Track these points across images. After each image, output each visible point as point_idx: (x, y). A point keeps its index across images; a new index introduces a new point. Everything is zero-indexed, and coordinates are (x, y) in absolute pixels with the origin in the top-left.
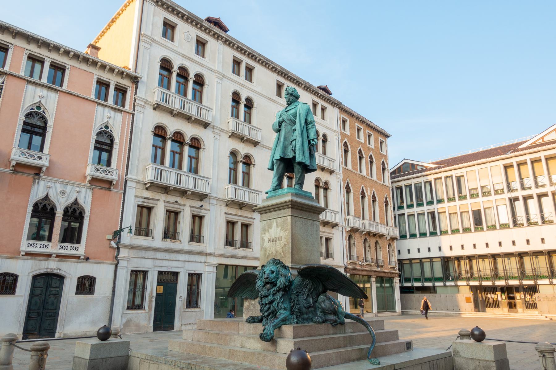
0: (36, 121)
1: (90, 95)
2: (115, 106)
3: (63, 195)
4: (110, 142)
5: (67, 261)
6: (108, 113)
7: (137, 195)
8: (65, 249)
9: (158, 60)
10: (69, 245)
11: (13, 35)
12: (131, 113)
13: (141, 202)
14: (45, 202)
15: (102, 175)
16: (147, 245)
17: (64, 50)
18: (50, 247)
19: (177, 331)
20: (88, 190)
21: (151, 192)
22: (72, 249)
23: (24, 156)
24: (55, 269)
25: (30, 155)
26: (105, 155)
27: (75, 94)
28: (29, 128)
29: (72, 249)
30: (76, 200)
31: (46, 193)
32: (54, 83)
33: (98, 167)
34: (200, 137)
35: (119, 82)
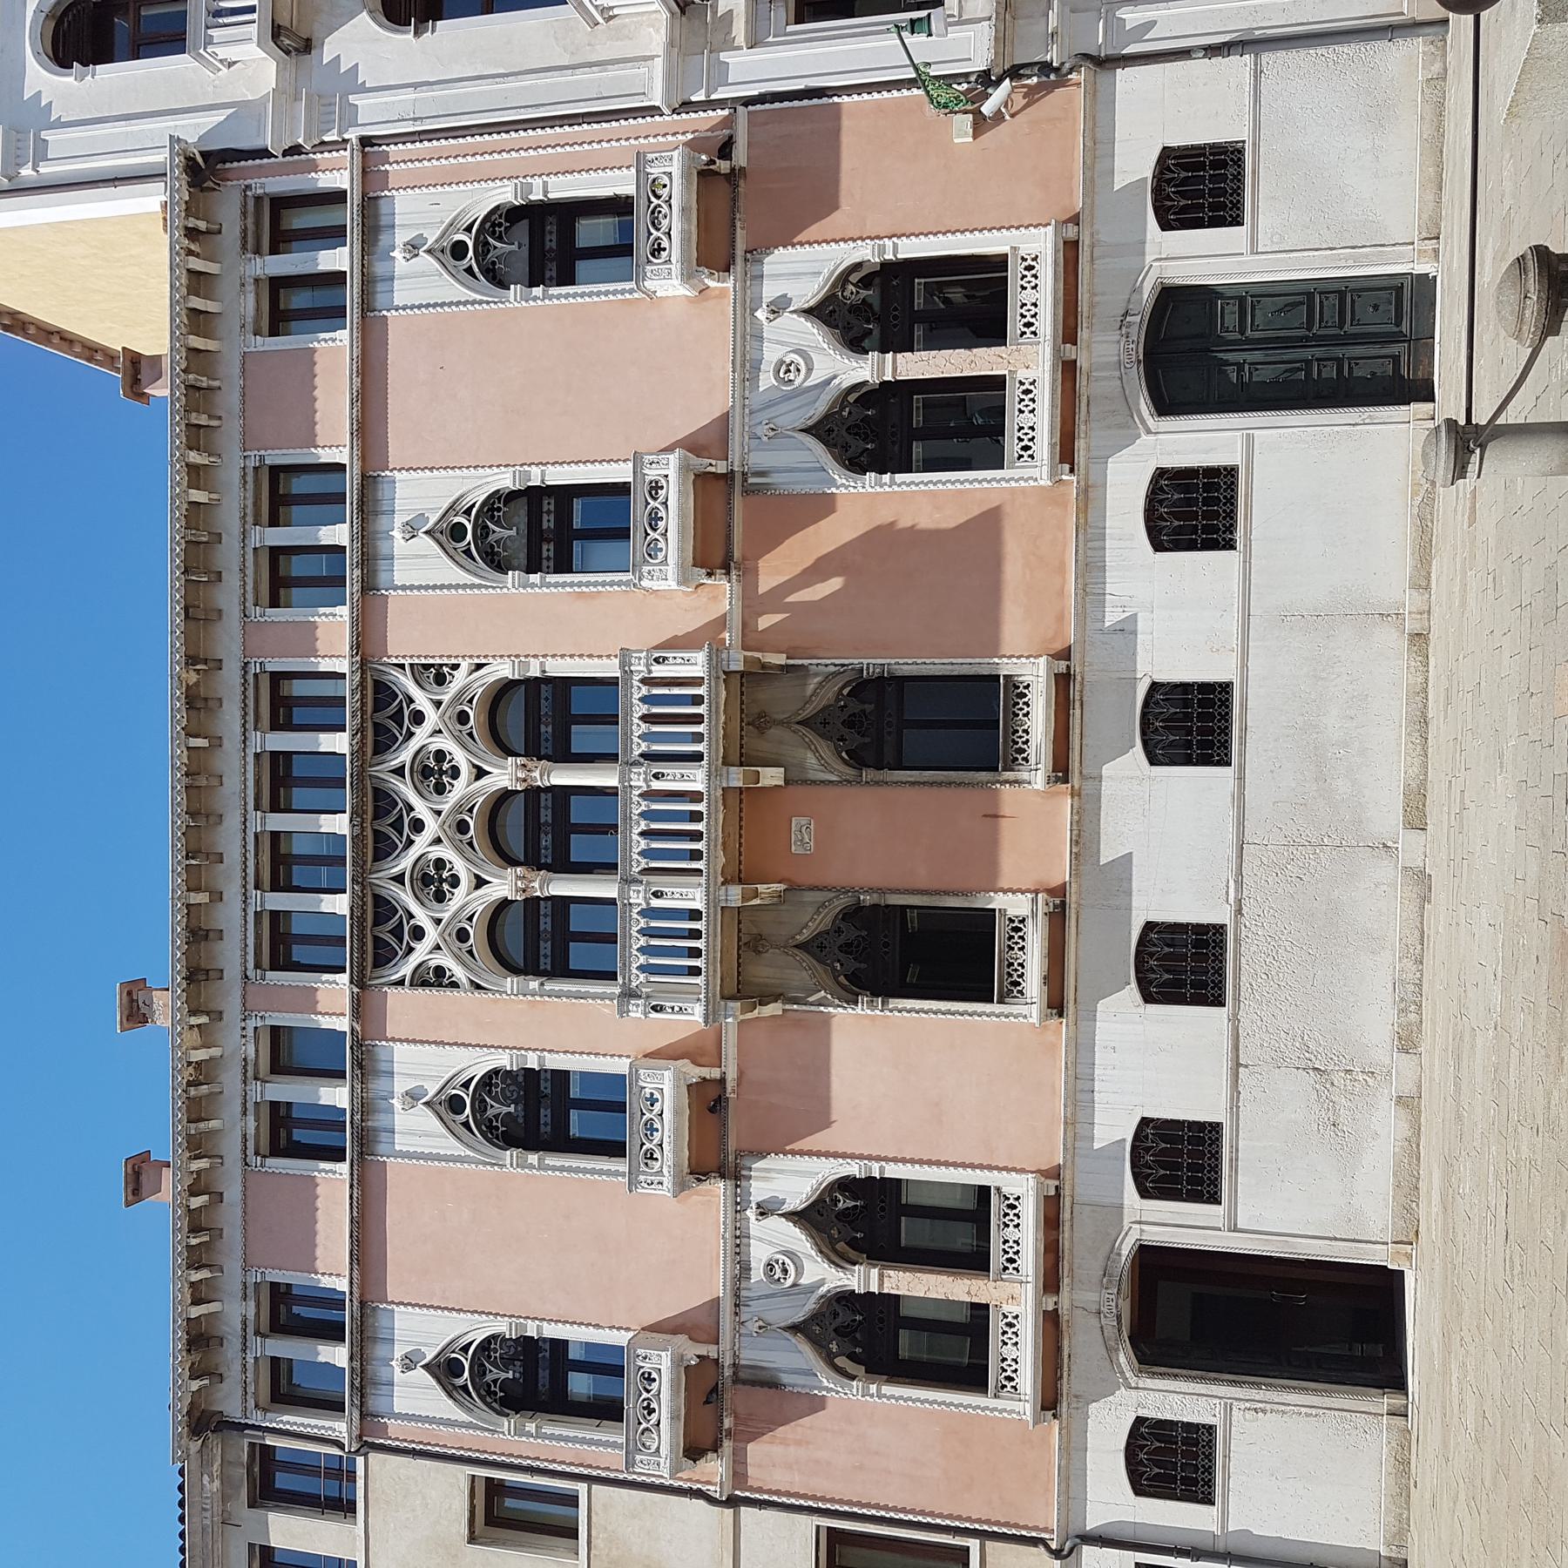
0: (514, 719)
2: (353, 234)
3: (798, 370)
4: (525, 224)
8: (1032, 434)
9: (71, 79)
10: (1012, 420)
15: (677, 225)
18: (1015, 1310)
19: (1244, 665)
22: (1032, 406)
23: (661, 545)
25: (650, 525)
26: (591, 232)
28: (548, 550)
29: (1032, 406)
30: (809, 312)
32: (340, 498)
33: (642, 247)
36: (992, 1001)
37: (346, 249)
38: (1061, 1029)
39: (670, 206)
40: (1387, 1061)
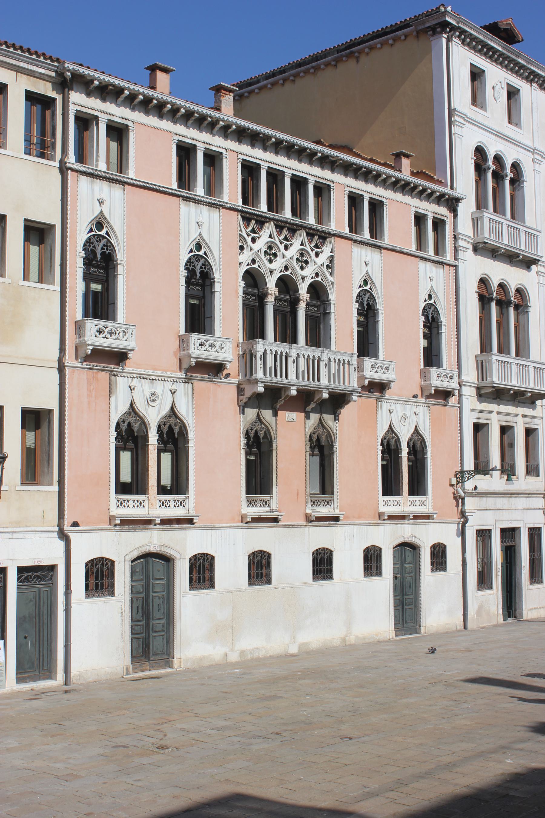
1: (345, 229)
8: (168, 506)
12: (452, 266)
14: (416, 437)
16: (486, 488)
22: (177, 506)
24: (410, 536)
27: (398, 249)
29: (177, 506)
36: (246, 494)
37: (203, 195)
39: (115, 339)
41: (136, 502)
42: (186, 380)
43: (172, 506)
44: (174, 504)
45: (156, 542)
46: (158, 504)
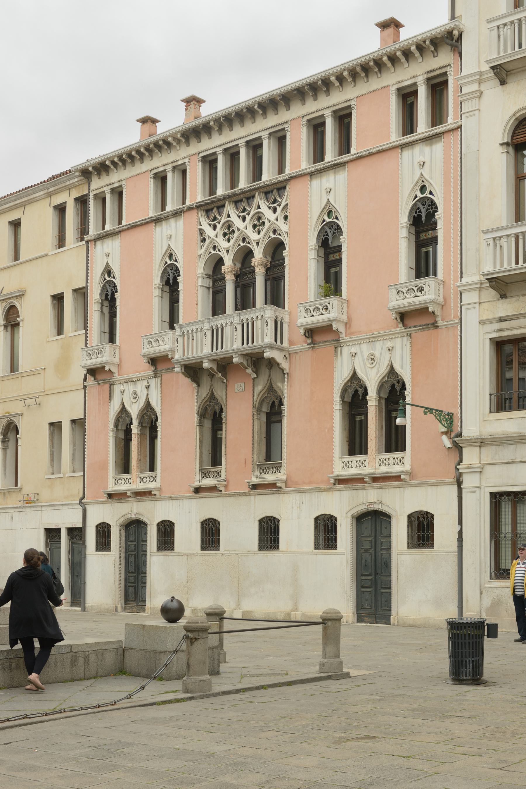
5: (389, 487)
6: (327, 183)
7: (485, 317)
11: (129, 161)
13: (495, 331)
14: (392, 380)
17: (80, 172)
19: (179, 555)
20: (405, 339)
21: (514, 299)
23: (413, 295)
31: (351, 367)
34: (511, 118)
35: (430, 69)
38: (247, 490)
40: (190, 606)
41: (396, 459)
42: (156, 376)
43: (354, 466)
44: (390, 462)
45: (135, 511)
46: (341, 465)
